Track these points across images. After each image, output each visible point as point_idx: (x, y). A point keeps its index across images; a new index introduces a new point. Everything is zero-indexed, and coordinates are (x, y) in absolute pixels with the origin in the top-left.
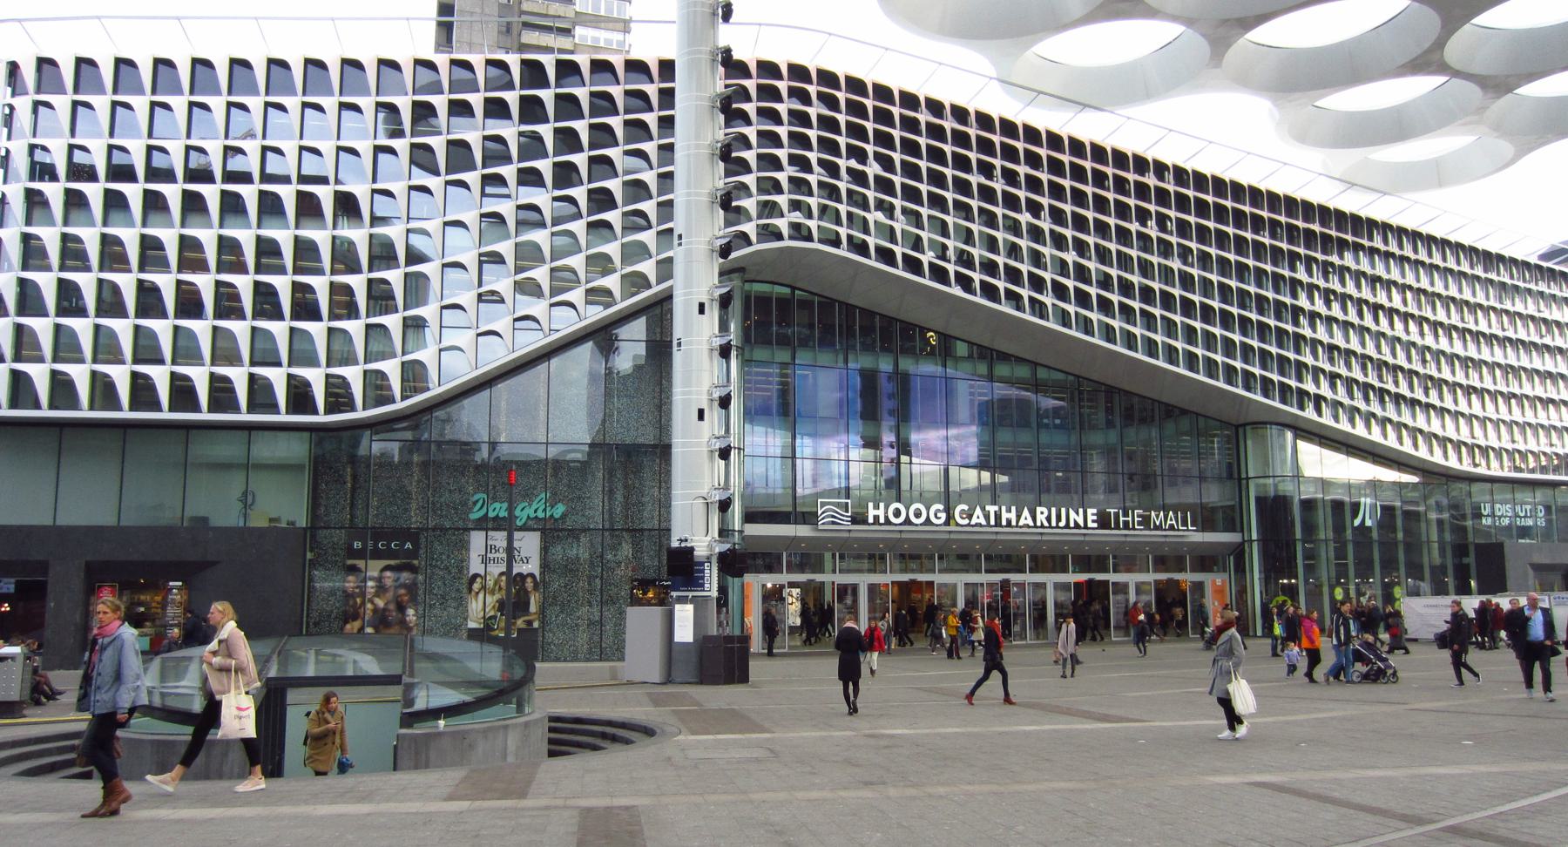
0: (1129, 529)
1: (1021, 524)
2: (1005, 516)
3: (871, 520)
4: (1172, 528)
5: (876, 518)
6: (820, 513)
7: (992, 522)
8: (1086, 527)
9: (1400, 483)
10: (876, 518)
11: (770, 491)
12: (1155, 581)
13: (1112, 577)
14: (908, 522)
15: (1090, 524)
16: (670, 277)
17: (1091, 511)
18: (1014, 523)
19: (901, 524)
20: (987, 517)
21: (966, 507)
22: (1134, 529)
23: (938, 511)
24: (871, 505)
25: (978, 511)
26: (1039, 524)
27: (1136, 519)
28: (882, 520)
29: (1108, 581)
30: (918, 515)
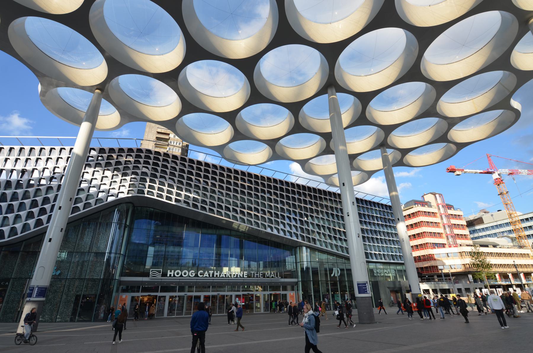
0: (258, 278)
1: (221, 276)
2: (215, 274)
3: (168, 275)
4: (272, 277)
5: (170, 275)
6: (150, 273)
7: (211, 276)
8: (243, 277)
9: (146, 257)
10: (170, 275)
11: (289, 269)
12: (270, 294)
13: (159, 294)
14: (181, 276)
15: (245, 276)
16: (56, 202)
17: (245, 272)
18: (218, 276)
19: (179, 277)
20: (209, 275)
21: (202, 271)
22: (260, 278)
23: (192, 273)
24: (169, 271)
25: (206, 272)
26: (227, 276)
27: (261, 275)
28: (172, 276)
29: (157, 295)
30: (185, 274)
